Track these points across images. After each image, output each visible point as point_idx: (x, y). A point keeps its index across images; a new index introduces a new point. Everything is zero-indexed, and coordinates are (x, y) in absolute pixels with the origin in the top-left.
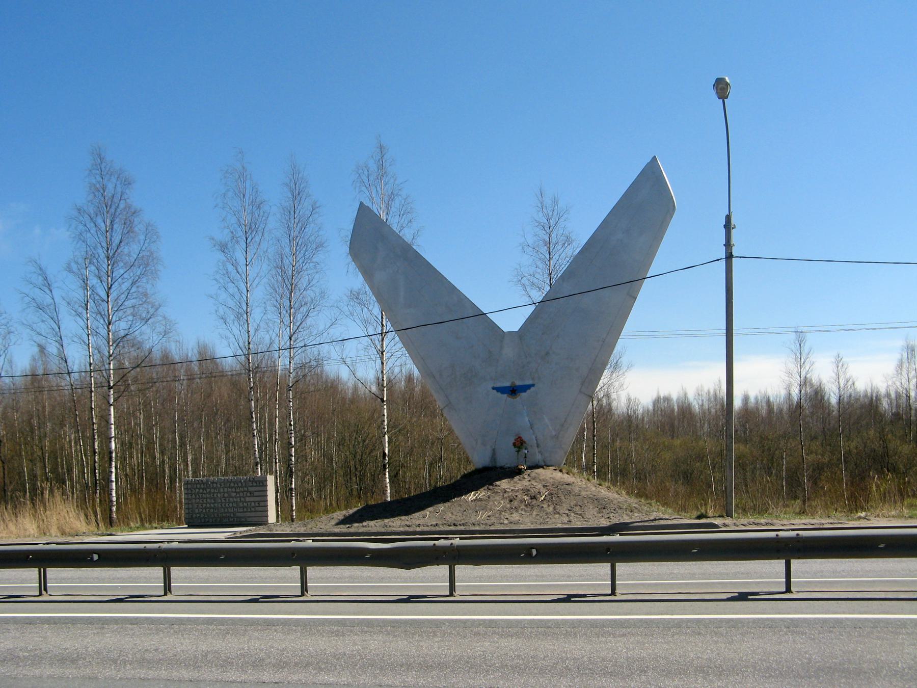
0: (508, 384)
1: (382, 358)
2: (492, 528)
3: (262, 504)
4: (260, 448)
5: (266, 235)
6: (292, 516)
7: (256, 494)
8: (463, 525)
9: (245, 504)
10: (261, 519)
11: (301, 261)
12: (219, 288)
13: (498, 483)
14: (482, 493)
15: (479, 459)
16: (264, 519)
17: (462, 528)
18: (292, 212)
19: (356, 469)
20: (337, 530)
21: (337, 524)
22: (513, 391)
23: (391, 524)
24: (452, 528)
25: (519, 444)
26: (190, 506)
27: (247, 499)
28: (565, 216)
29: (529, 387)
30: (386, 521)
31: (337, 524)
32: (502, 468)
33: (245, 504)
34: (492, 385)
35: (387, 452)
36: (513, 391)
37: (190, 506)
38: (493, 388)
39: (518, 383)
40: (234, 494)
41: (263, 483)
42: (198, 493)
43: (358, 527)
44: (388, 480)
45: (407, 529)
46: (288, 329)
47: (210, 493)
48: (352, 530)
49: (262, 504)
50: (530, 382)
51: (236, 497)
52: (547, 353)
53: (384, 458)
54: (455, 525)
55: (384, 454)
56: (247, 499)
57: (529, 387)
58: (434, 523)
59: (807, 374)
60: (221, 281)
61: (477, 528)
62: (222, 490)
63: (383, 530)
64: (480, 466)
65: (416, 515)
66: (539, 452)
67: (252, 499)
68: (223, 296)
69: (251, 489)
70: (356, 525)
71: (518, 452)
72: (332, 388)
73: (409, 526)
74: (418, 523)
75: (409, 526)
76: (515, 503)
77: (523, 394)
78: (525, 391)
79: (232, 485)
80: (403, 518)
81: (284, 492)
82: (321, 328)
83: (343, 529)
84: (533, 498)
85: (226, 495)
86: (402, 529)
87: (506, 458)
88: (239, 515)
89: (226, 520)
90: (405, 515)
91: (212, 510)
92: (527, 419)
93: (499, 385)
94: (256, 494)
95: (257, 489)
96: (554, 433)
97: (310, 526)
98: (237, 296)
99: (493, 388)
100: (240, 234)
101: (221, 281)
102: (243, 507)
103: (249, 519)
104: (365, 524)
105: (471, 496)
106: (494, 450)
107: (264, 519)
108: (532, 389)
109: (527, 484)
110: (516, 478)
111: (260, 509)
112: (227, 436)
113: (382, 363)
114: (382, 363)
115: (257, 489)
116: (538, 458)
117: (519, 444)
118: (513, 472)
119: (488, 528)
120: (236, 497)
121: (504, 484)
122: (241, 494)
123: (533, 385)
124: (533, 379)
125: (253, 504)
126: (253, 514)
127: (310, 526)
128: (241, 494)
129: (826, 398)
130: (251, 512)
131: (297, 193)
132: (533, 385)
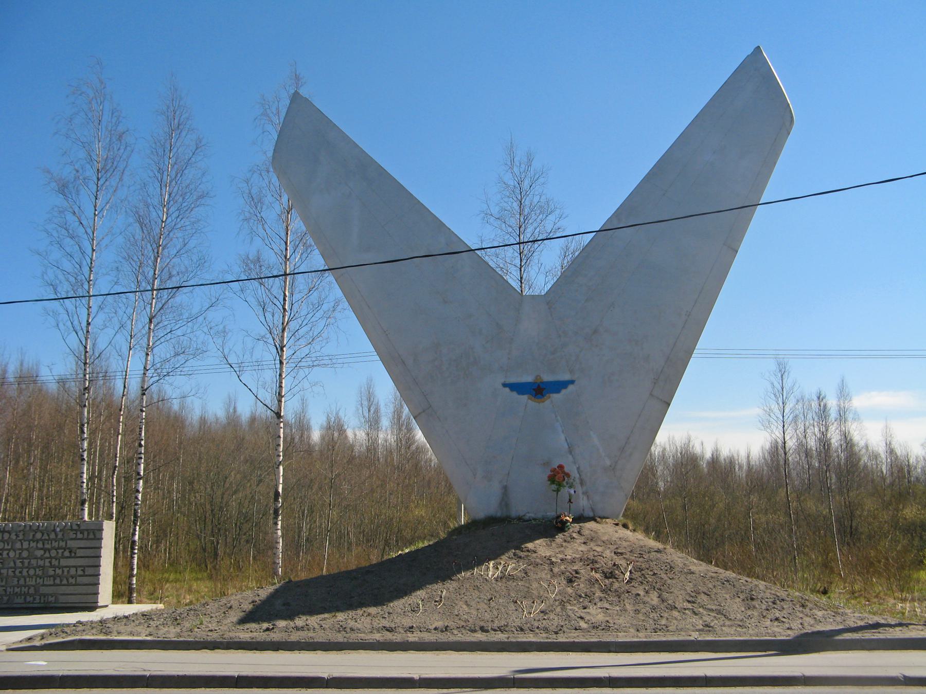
0: (529, 379)
1: (281, 356)
2: (562, 638)
3: (89, 571)
4: (91, 479)
5: (125, 178)
6: (131, 584)
7: (80, 553)
8: (501, 629)
9: (59, 571)
11: (174, 216)
12: (51, 243)
13: (530, 545)
14: (509, 564)
15: (473, 502)
16: (90, 598)
17: (500, 637)
18: (167, 151)
19: (214, 516)
20: (245, 634)
21: (242, 621)
22: (539, 390)
23: (352, 623)
24: (480, 637)
25: (558, 477)
27: (63, 562)
28: (541, 180)
29: (563, 385)
30: (341, 616)
31: (242, 621)
32: (520, 519)
33: (59, 571)
34: (502, 381)
35: (280, 490)
36: (539, 390)
38: (505, 385)
39: (547, 378)
40: (39, 553)
41: (95, 534)
43: (286, 630)
44: (279, 533)
45: (389, 636)
46: (148, 309)
48: (275, 636)
49: (89, 571)
50: (567, 377)
51: (42, 558)
52: (595, 331)
53: (276, 500)
54: (483, 629)
55: (277, 494)
56: (63, 562)
57: (563, 385)
58: (439, 624)
60: (55, 234)
61: (531, 638)
62: (18, 545)
63: (340, 638)
64: (481, 515)
65: (398, 605)
66: (585, 493)
67: (72, 562)
68: (56, 254)
69: (71, 544)
70: (282, 623)
71: (558, 491)
72: (177, 422)
73: (390, 630)
74: (407, 622)
75: (390, 630)
76: (582, 587)
77: (555, 396)
78: (558, 391)
79: (39, 535)
80: (373, 610)
81: (123, 545)
82: (195, 311)
83: (254, 631)
84: (609, 575)
86: (377, 636)
87: (529, 502)
88: (44, 590)
89: (20, 600)
90: (375, 605)
92: (563, 437)
93: (513, 380)
94: (80, 553)
95: (82, 544)
96: (608, 463)
97: (187, 625)
98: (77, 256)
99: (505, 385)
100: (91, 173)
101: (55, 234)
102: (54, 577)
103: (62, 599)
104: (300, 621)
105: (491, 570)
106: (505, 489)
107: (90, 598)
108: (571, 388)
109: (583, 548)
110: (559, 538)
111: (85, 580)
112: (44, 469)
113: (281, 363)
114: (281, 363)
115: (82, 544)
116: (583, 503)
117: (558, 477)
118: (553, 527)
119: (553, 638)
120: (42, 558)
121: (540, 547)
122: (53, 553)
123: (572, 382)
124: (572, 372)
125: (73, 571)
127: (187, 625)
130: (68, 585)
131: (176, 122)
132: (572, 382)
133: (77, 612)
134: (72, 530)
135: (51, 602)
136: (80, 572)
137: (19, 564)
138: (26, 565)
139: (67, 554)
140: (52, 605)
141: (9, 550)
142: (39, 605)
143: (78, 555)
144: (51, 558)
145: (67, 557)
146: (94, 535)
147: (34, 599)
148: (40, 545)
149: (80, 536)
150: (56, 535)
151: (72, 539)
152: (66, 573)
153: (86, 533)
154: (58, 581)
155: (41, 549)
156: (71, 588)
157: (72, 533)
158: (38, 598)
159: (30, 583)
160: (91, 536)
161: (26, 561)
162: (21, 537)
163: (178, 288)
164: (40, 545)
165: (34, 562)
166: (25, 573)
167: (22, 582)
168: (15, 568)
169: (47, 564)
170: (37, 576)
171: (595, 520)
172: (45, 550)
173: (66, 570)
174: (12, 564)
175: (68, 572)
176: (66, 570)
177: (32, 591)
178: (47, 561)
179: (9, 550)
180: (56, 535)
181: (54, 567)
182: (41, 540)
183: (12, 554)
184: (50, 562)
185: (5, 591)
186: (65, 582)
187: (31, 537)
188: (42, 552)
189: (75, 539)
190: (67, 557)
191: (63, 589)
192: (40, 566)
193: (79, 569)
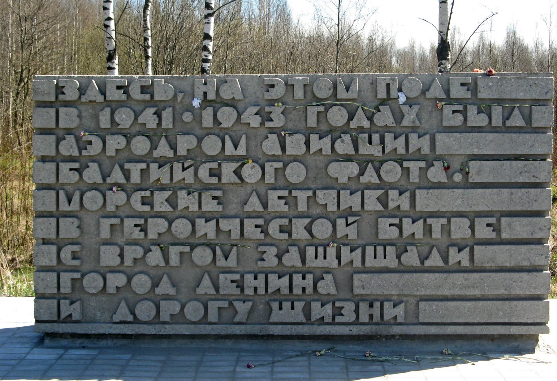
7: (480, 172)
10: (500, 311)
16: (524, 311)
26: (69, 229)
27: (426, 201)
37: (69, 229)
40: (344, 171)
42: (124, 159)
47: (193, 159)
51: (357, 188)
56: (426, 201)
59: (382, 40)
62: (271, 146)
79: (338, 117)
85: (296, 173)
88: (363, 284)
91: (202, 256)
94: (480, 172)
95: (490, 144)
107: (524, 311)
111: (503, 255)
115: (490, 144)
120: (357, 188)
122: (392, 172)
125: (460, 229)
126: (456, 283)
128: (392, 172)
129: (294, 21)
133: (486, 356)
134: (449, 100)
135: (394, 321)
136: (483, 232)
137: (275, 203)
138: (302, 206)
139: (436, 174)
140: (396, 330)
141: (242, 160)
142: (356, 330)
143: (474, 178)
144: (383, 186)
145: (439, 186)
146: (528, 119)
147: (338, 312)
148: (344, 146)
149: (476, 119)
150: (399, 117)
151: (450, 130)
152: (436, 234)
153: (497, 111)
154: (411, 258)
155: (348, 159)
156: (459, 278)
157: (448, 110)
158: (349, 307)
159: (320, 262)
160: (517, 121)
161: (302, 196)
162: (278, 121)
163: (339, 9)
164: (344, 146)
165: (326, 197)
166: (299, 231)
167: (292, 259)
168: (265, 217)
169: (372, 205)
170: (344, 242)
171: (245, 164)
172: (364, 164)
173: (436, 224)
174: (254, 204)
175: (446, 230)
176: (436, 224)
177: (327, 286)
178: (372, 196)
179: (242, 160)
180: (399, 117)
181: (398, 213)
182: (345, 129)
183: (251, 173)
184: (383, 201)
185: (241, 286)
186: (435, 260)
187: (312, 122)
188: (353, 168)
189: (466, 129)
190: (439, 186)
191: (429, 283)
192: (350, 212)
193: (481, 223)
